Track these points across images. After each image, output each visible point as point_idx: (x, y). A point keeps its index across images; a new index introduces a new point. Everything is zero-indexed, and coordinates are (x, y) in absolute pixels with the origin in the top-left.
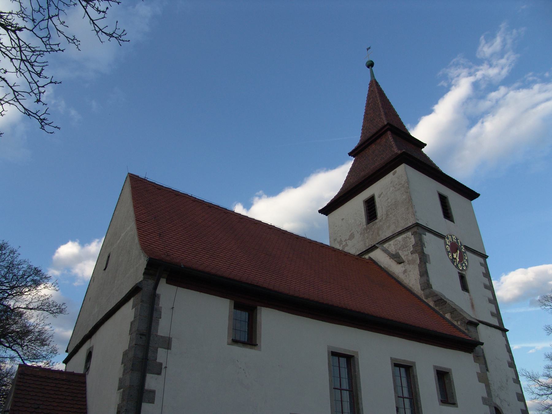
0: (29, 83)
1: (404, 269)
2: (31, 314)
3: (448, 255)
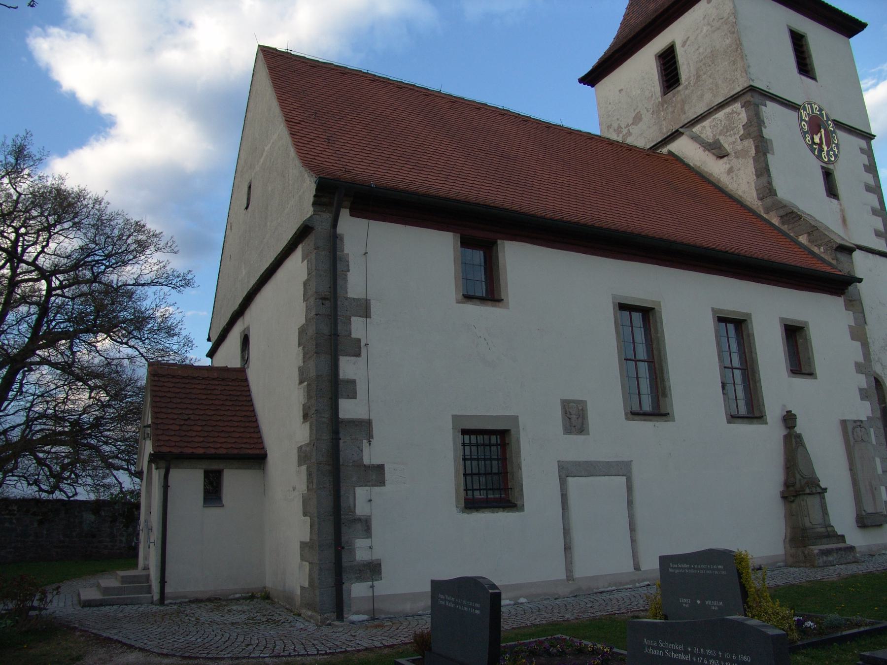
1: (728, 166)
3: (805, 138)
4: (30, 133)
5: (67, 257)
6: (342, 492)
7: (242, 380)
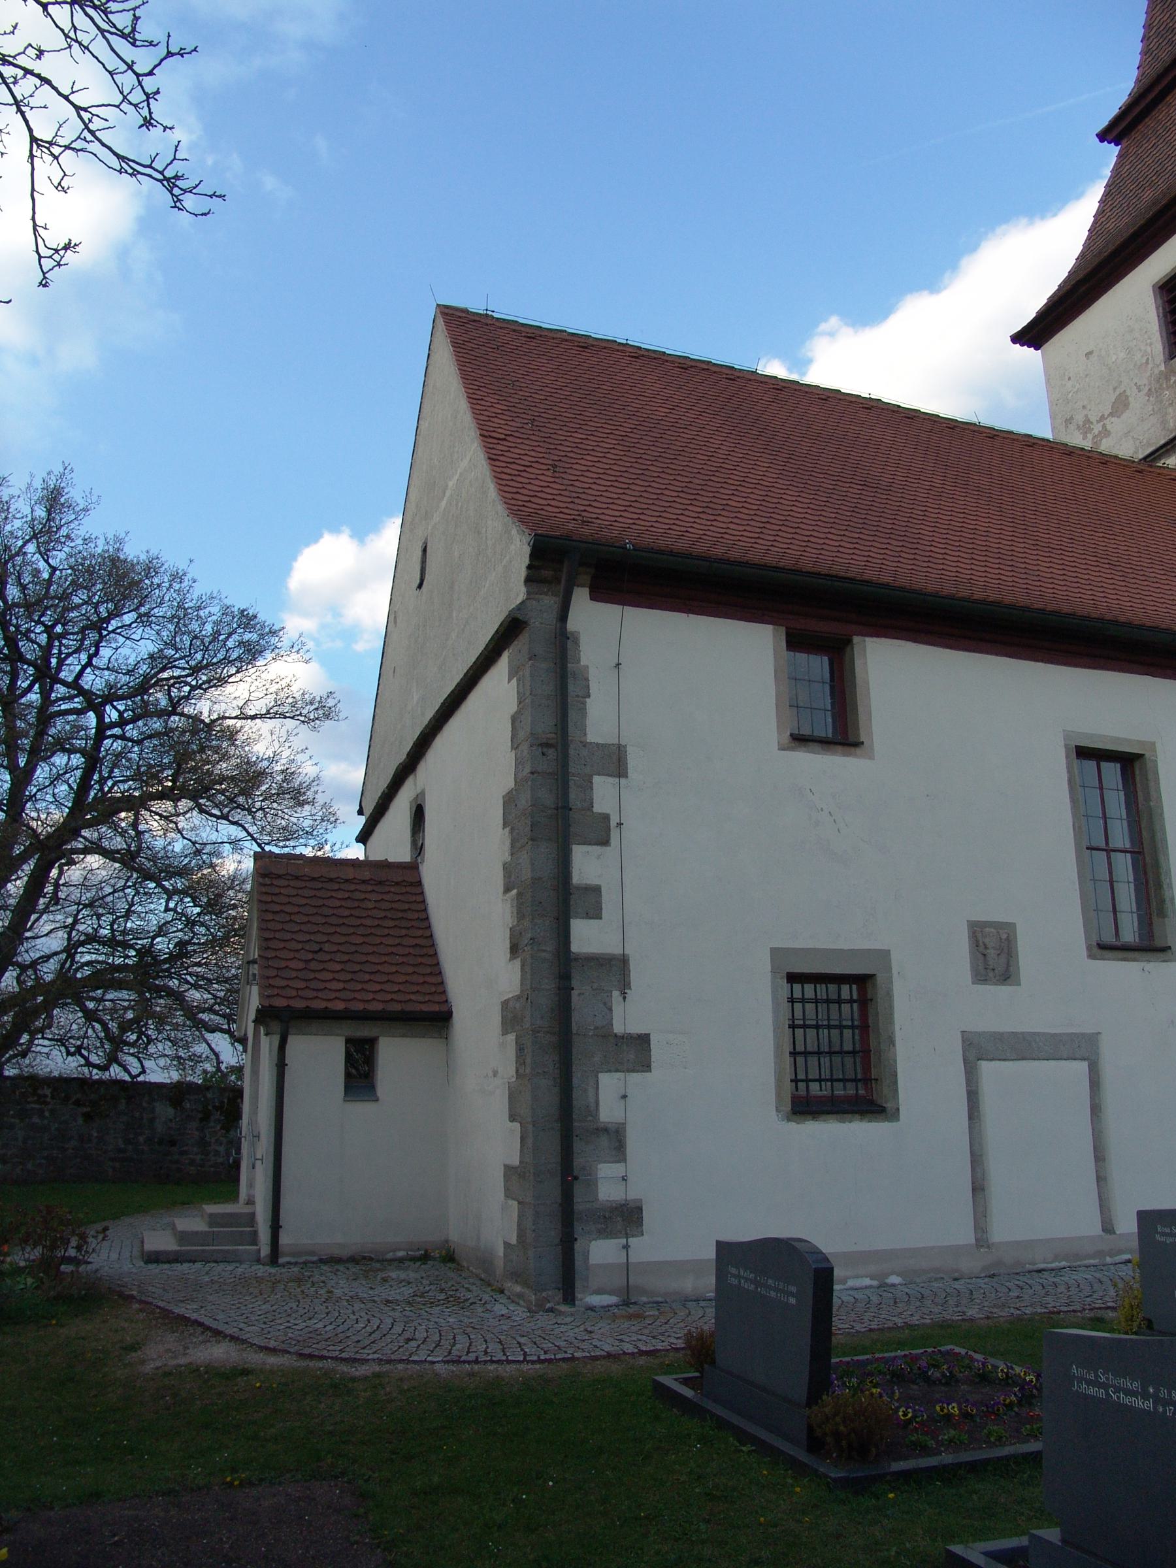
0: (111, 73)
2: (254, 730)
4: (69, 468)
5: (129, 672)
6: (575, 1081)
7: (411, 884)
